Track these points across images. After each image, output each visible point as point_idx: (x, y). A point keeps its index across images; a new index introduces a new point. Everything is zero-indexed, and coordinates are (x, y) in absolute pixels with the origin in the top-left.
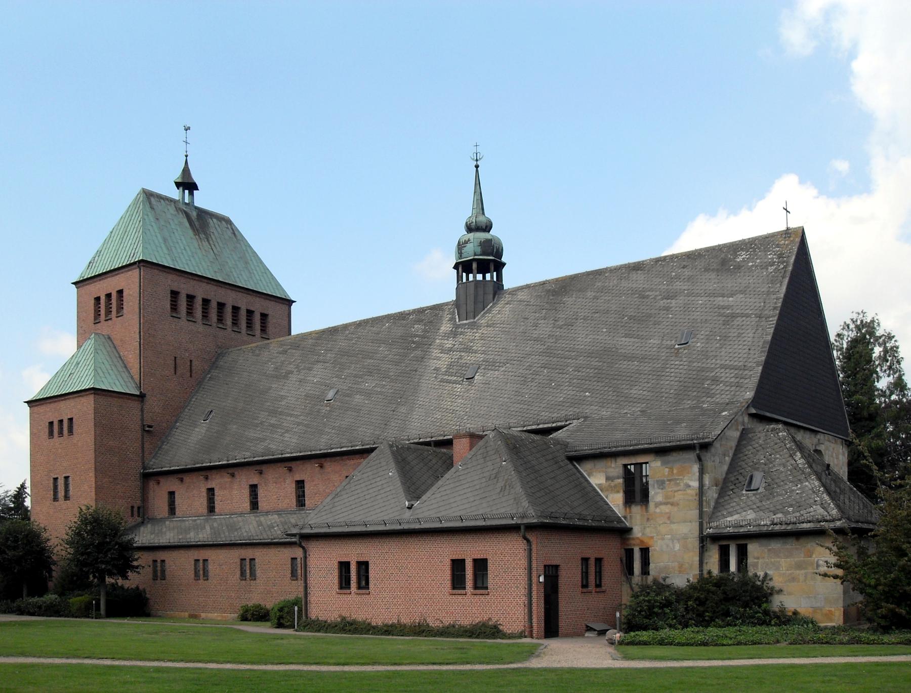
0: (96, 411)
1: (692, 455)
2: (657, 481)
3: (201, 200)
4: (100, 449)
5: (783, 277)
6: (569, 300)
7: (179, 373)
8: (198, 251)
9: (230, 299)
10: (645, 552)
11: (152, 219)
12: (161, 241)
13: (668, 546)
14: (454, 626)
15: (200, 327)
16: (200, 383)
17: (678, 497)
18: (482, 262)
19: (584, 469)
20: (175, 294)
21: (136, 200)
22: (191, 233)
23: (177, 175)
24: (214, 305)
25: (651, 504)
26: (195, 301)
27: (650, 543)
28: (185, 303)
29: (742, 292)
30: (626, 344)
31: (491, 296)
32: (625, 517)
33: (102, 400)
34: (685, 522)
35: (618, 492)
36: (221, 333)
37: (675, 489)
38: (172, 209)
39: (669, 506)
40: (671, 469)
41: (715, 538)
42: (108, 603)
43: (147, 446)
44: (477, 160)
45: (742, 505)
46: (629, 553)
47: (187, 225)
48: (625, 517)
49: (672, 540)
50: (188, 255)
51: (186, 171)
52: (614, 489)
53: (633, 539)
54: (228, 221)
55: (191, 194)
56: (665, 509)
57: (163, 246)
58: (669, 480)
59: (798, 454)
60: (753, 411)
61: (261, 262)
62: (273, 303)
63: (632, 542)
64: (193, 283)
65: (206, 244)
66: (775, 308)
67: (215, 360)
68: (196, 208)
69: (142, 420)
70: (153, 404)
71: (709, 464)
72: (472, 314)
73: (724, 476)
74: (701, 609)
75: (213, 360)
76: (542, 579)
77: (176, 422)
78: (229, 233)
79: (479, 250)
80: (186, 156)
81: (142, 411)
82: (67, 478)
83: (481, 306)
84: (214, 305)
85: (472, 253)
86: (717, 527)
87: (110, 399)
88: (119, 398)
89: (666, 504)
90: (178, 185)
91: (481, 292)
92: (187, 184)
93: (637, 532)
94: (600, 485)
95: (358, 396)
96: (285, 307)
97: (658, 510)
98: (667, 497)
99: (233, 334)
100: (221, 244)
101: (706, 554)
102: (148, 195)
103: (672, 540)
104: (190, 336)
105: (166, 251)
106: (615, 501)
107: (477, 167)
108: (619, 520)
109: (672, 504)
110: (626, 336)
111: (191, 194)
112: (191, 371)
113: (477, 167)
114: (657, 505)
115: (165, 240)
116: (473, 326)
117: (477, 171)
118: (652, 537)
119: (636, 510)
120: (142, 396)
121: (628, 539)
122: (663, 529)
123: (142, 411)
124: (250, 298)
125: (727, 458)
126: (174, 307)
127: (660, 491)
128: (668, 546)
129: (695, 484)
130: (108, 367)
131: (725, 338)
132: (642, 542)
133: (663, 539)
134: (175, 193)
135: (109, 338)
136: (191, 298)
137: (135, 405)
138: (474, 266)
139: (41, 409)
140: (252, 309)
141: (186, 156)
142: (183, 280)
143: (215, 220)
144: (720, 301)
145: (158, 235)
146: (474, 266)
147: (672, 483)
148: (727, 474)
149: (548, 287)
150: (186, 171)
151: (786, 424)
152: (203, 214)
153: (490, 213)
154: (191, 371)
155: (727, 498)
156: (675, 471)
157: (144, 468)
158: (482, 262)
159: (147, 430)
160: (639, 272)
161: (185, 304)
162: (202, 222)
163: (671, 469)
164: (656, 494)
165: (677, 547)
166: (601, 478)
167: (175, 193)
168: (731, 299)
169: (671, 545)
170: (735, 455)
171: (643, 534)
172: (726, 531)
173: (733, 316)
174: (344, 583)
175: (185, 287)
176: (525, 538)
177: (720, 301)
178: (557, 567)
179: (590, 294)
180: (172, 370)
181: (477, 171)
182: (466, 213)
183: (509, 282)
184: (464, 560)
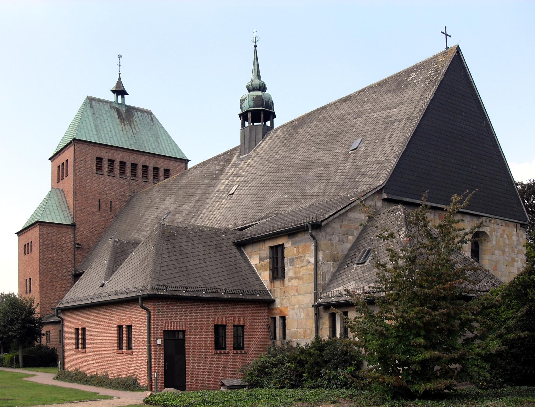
0: (41, 236)
1: (306, 236)
2: (290, 259)
3: (129, 101)
4: (42, 261)
5: (433, 86)
6: (301, 130)
7: (102, 209)
8: (121, 132)
9: (141, 161)
10: (283, 318)
11: (89, 113)
12: (93, 126)
13: (297, 314)
14: (118, 379)
15: (118, 180)
16: (117, 216)
17: (303, 271)
18: (258, 114)
19: (248, 251)
20: (99, 160)
21: (85, 104)
22: (118, 121)
23: (113, 85)
24: (128, 165)
25: (286, 279)
26: (115, 163)
27: (286, 312)
28: (152, 172)
29: (403, 103)
30: (322, 155)
31: (261, 136)
32: (271, 291)
33: (45, 228)
34: (307, 293)
35: (266, 270)
36: (134, 183)
37: (301, 265)
38: (107, 108)
39: (297, 280)
40: (298, 248)
41: (327, 307)
42: (24, 357)
43: (78, 257)
44: (255, 42)
45: (350, 277)
46: (274, 319)
47: (116, 116)
48: (271, 291)
49: (299, 309)
50: (114, 135)
51: (119, 83)
52: (262, 268)
53: (276, 309)
54: (149, 113)
55: (123, 97)
56: (295, 282)
57: (94, 130)
58: (297, 258)
59: (404, 229)
60: (385, 196)
61: (169, 137)
62: (173, 162)
63: (275, 311)
64: (113, 152)
65: (128, 128)
66: (420, 111)
67: (129, 201)
68: (126, 106)
69: (75, 241)
70: (83, 231)
71: (323, 242)
72: (247, 150)
73: (346, 252)
74: (301, 369)
75: (128, 200)
76: (159, 342)
77: (100, 241)
78: (149, 120)
79: (252, 104)
80: (120, 74)
81: (75, 235)
82: (30, 279)
83: (254, 143)
84: (128, 165)
85: (248, 107)
86: (326, 298)
87: (51, 228)
88: (58, 227)
89: (295, 278)
90: (114, 92)
91: (254, 133)
92: (120, 92)
93: (278, 304)
94: (256, 265)
95: (177, 215)
96: (183, 165)
97: (290, 284)
98: (295, 273)
99: (143, 184)
100: (140, 127)
101: (321, 321)
102: (90, 100)
103: (299, 309)
104: (110, 186)
105: (95, 133)
106: (265, 276)
107: (255, 46)
108: (266, 293)
109: (299, 279)
110: (325, 149)
111: (123, 97)
112: (111, 208)
113: (255, 46)
114: (290, 279)
115: (96, 126)
116: (247, 158)
117: (256, 50)
118: (287, 307)
119: (277, 283)
120: (73, 226)
121: (273, 309)
122: (293, 300)
123: (75, 235)
124: (156, 160)
125: (350, 237)
126: (99, 168)
127: (291, 267)
128: (297, 314)
129: (312, 260)
130: (55, 208)
131: (381, 140)
132: (281, 311)
133: (294, 309)
134: (112, 97)
135: (62, 191)
136: (145, 168)
137: (69, 232)
138: (249, 115)
139: (23, 237)
140: (157, 166)
141: (120, 74)
142: (105, 150)
143: (139, 113)
144: (387, 113)
145: (92, 124)
146: (249, 115)
147: (299, 260)
148: (350, 250)
149: (294, 124)
150: (119, 83)
151: (405, 203)
152: (130, 110)
153: (264, 78)
154: (111, 208)
155: (342, 271)
156: (300, 250)
157: (75, 271)
158: (258, 114)
159: (78, 247)
160: (347, 102)
161: (113, 166)
162: (128, 115)
163: (298, 248)
164: (289, 270)
165: (303, 315)
166: (257, 258)
167: (112, 97)
168: (395, 110)
169: (299, 314)
170: (361, 234)
171: (282, 305)
172: (330, 301)
173: (392, 123)
174: (219, 345)
175: (106, 155)
176: (142, 307)
177: (387, 113)
178: (85, 328)
179: (314, 124)
180: (97, 209)
181: (256, 50)
182: (248, 78)
183: (276, 126)
184: (122, 326)
